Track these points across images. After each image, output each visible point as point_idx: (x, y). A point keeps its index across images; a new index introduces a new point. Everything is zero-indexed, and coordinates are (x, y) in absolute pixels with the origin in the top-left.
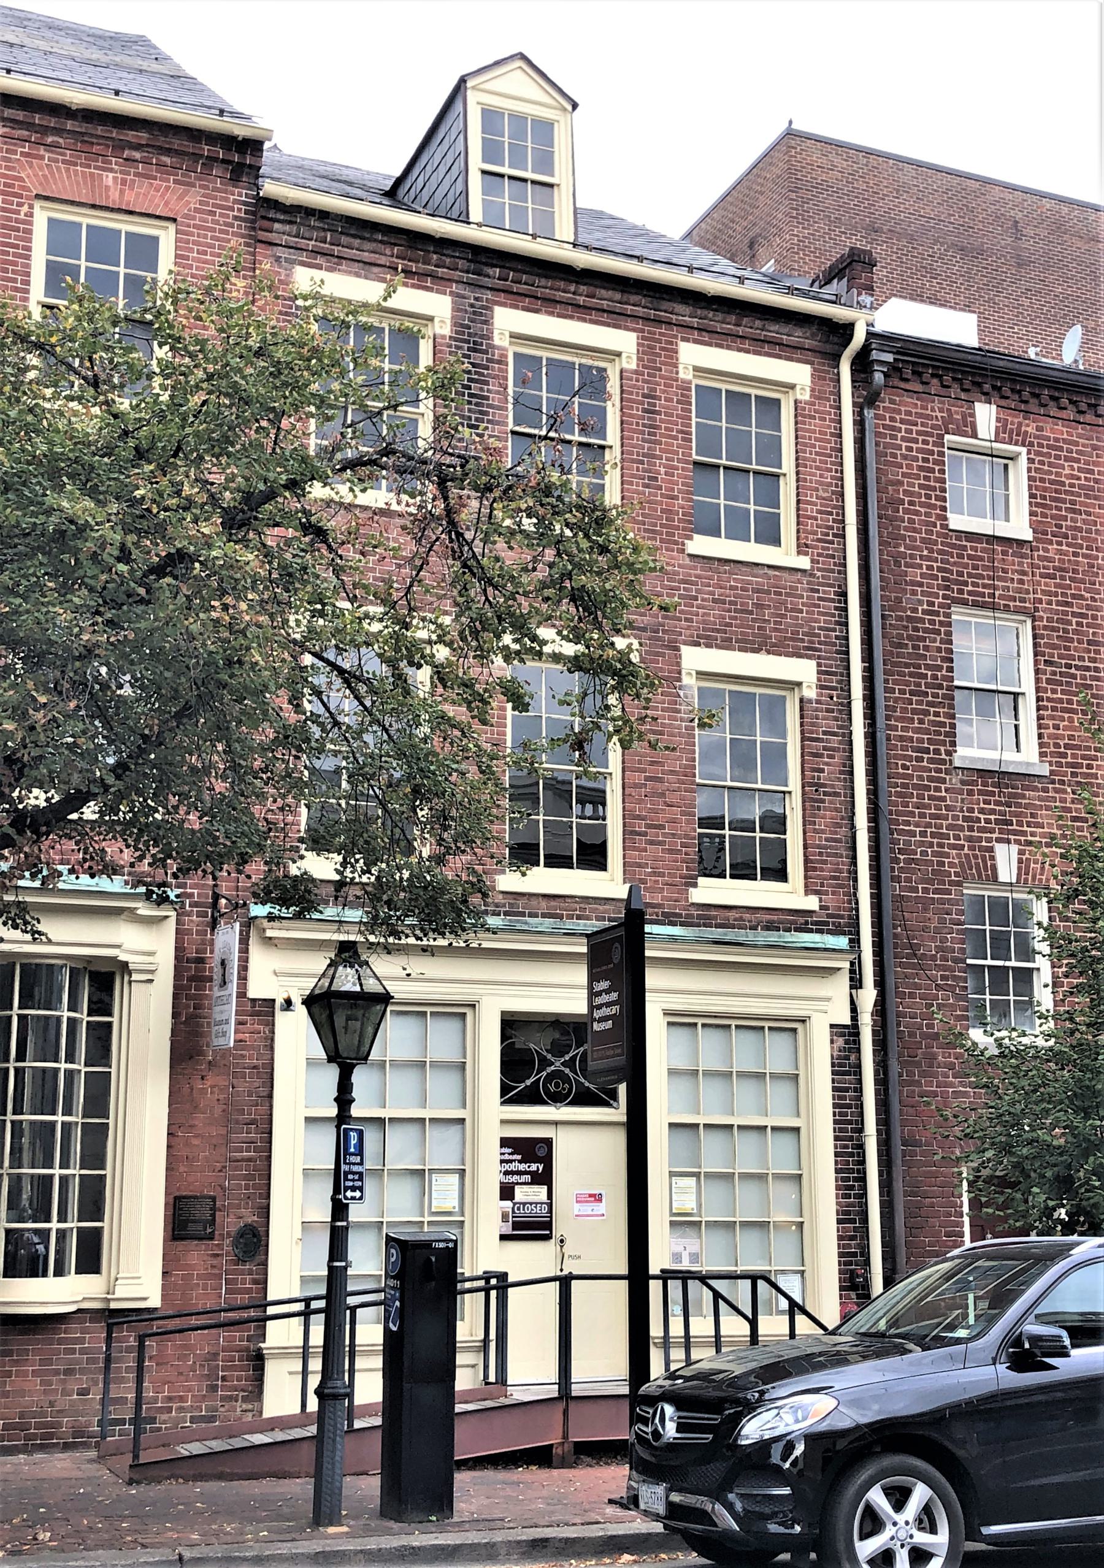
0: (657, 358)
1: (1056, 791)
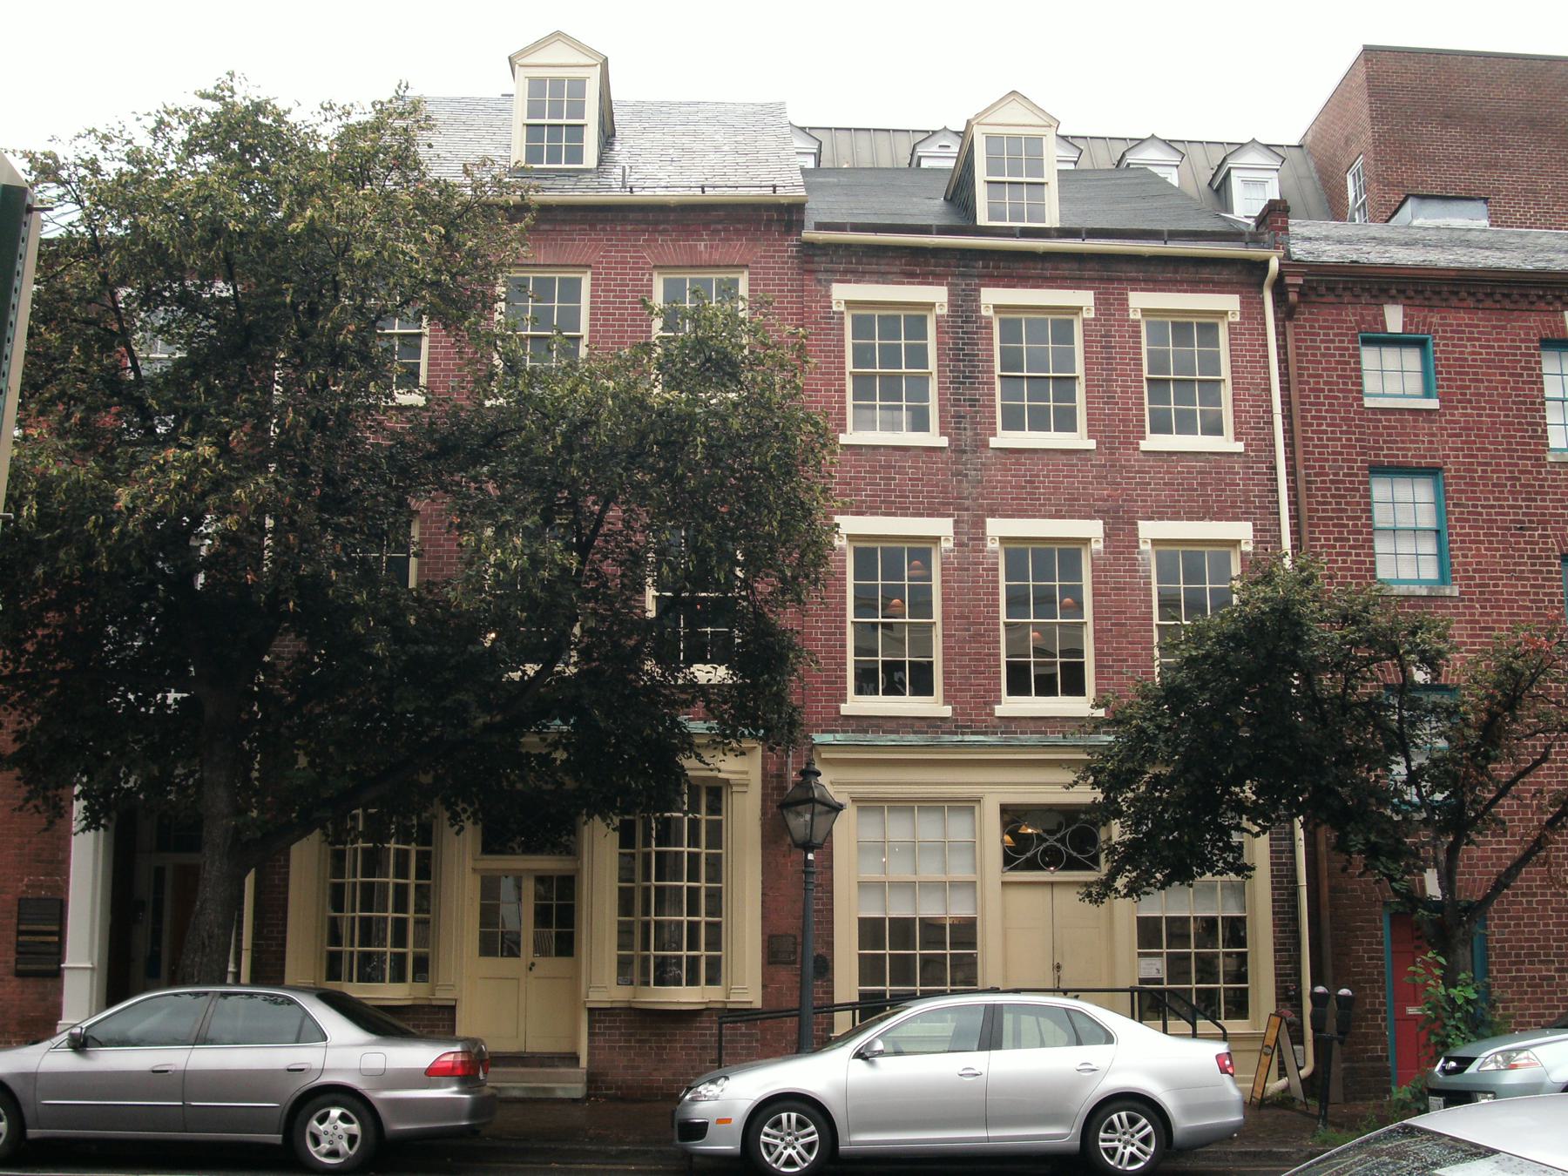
0: (1111, 305)
1: (1465, 607)
